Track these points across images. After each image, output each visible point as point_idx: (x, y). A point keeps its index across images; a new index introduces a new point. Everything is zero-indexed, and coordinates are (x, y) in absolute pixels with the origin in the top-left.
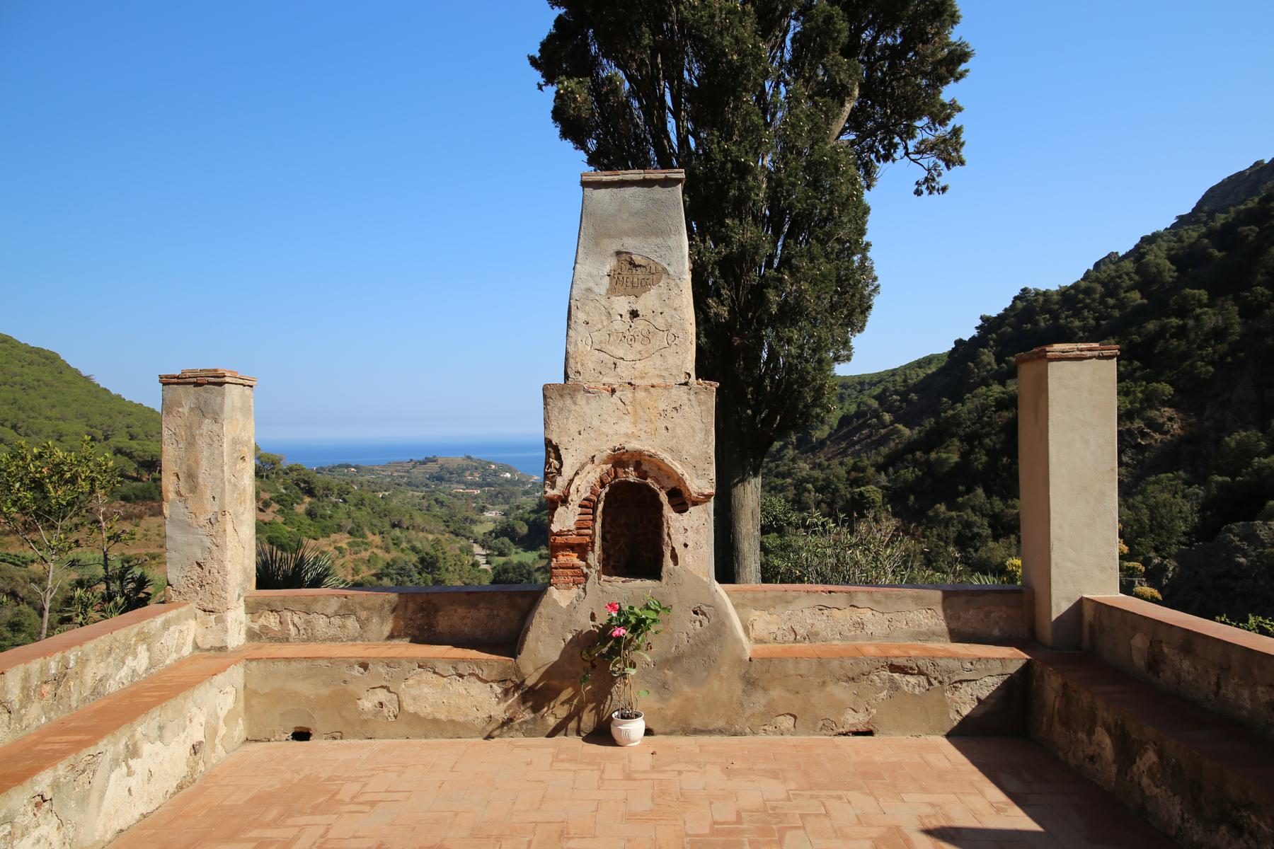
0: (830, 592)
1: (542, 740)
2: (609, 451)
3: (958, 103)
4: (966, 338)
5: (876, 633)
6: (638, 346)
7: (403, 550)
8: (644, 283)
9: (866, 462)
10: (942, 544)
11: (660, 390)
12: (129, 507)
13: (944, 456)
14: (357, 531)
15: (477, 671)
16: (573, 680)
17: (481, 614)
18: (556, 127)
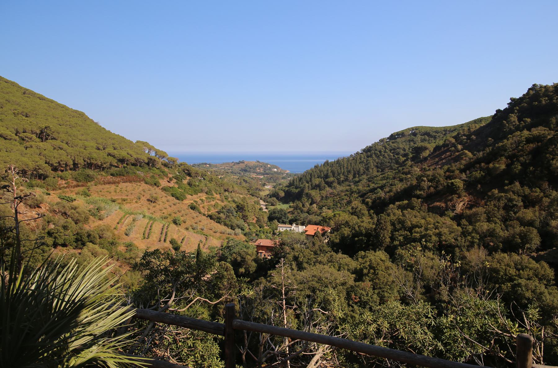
4: (502, 109)
7: (229, 202)
10: (496, 209)
12: (114, 179)
13: (497, 166)
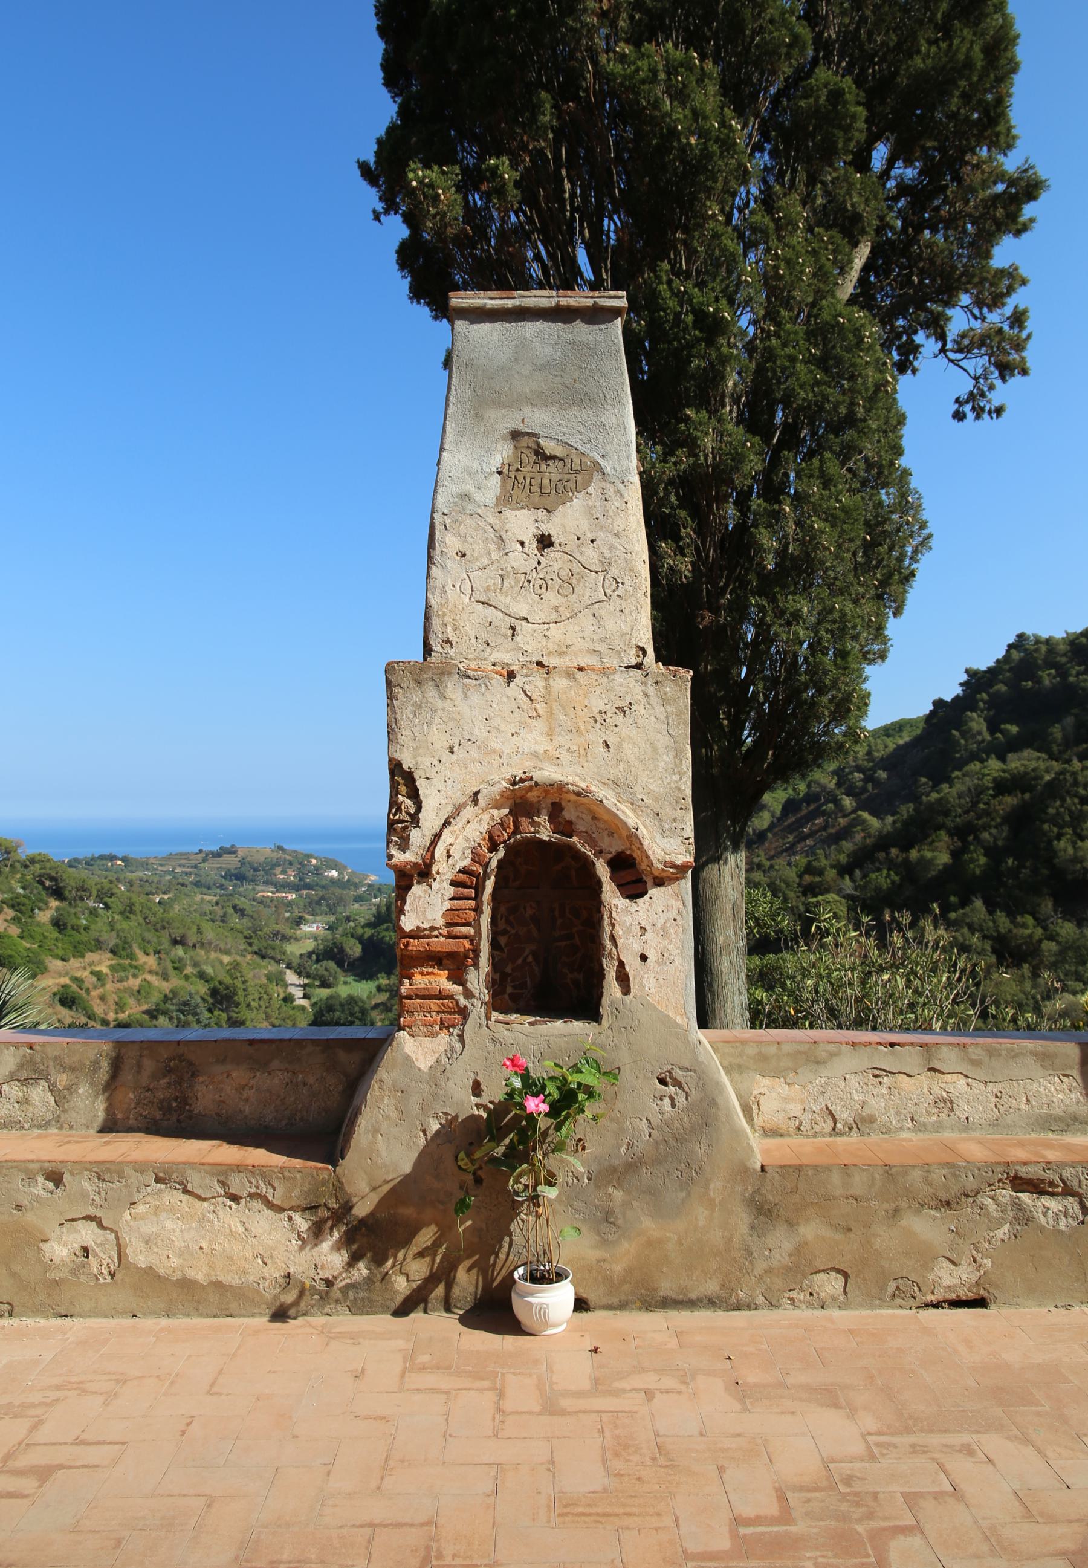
0: (892, 1045)
1: (386, 1321)
2: (505, 784)
3: (1021, 271)
4: (948, 698)
5: (975, 1118)
6: (552, 597)
7: (187, 978)
8: (561, 488)
9: (824, 862)
11: (594, 676)
13: (929, 855)
14: (124, 949)
15: (264, 1189)
16: (441, 1207)
17: (273, 1080)
18: (404, 277)
